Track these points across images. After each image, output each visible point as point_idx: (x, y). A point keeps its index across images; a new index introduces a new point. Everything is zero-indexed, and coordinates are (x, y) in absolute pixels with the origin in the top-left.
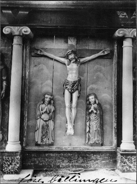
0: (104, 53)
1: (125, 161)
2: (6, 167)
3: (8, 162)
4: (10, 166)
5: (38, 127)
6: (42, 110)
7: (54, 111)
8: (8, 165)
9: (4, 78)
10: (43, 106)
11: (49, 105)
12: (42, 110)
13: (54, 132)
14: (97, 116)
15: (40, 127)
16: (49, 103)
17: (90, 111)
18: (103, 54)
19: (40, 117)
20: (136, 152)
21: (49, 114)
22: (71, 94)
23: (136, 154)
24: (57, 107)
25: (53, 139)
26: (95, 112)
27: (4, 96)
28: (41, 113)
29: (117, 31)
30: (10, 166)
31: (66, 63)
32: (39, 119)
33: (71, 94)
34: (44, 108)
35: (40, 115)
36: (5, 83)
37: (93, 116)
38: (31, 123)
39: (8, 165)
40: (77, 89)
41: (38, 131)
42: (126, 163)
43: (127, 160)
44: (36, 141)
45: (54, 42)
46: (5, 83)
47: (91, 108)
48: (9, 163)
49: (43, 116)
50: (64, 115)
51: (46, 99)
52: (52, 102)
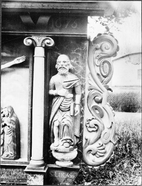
43: (33, 177)
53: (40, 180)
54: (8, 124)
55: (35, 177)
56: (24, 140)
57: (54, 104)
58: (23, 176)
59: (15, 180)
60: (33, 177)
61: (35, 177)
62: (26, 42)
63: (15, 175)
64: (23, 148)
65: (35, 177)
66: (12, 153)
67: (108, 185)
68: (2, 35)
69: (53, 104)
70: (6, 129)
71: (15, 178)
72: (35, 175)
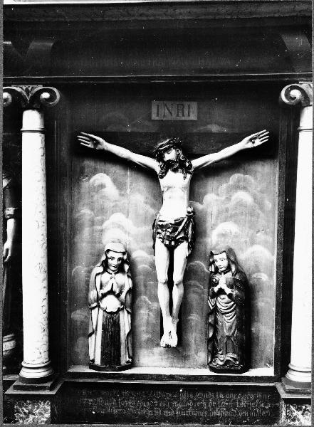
0: (254, 143)
1: (295, 414)
2: (21, 418)
3: (24, 408)
4: (31, 416)
5: (94, 328)
6: (101, 288)
7: (133, 292)
8: (25, 413)
9: (10, 211)
10: (106, 277)
11: (120, 275)
12: (101, 288)
13: (133, 338)
14: (233, 303)
15: (98, 328)
16: (120, 269)
17: (216, 289)
18: (250, 145)
19: (99, 306)
20: (310, 397)
21: (118, 296)
22: (171, 250)
23: (309, 400)
24: (140, 278)
25: (129, 355)
26: (228, 291)
27: (9, 255)
28: (100, 295)
29: (287, 86)
30: (31, 416)
31: (158, 170)
32: (97, 309)
33: (171, 250)
34: (107, 283)
35: (99, 299)
36: (11, 224)
37: (224, 301)
38: (78, 315)
39: (25, 413)
40: (185, 238)
41: (93, 336)
42: (299, 420)
43: (301, 412)
44: (91, 358)
45: (80, 216)
46: (11, 224)
47: (218, 283)
48: (27, 411)
49: (104, 303)
50: (155, 298)
51: (110, 261)
52: (126, 267)
53: (43, 412)
54: (228, 291)
55: (304, 412)
56: (266, 330)
57: (4, 273)
58: (264, 409)
59: (246, 419)
60: (301, 412)
61: (304, 412)
62: (287, 95)
63: (246, 409)
64: (258, 344)
65: (305, 410)
66: (235, 356)
67: (297, 423)
68: (4, 136)
69: (6, 272)
70: (223, 302)
71: (246, 414)
72: (304, 407)
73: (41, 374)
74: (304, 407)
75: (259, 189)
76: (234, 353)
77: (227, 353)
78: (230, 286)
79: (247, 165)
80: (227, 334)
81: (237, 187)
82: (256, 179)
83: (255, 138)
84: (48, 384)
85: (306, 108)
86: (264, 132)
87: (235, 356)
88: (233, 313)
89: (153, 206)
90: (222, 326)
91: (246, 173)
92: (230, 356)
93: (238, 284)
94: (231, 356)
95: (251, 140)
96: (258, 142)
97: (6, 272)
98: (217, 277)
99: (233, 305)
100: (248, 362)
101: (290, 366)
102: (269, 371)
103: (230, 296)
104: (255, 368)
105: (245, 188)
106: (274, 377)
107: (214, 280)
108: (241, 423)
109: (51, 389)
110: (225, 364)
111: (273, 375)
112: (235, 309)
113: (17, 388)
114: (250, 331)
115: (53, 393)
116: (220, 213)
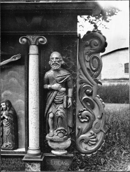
14: (8, 122)
18: (14, 60)
26: (6, 117)
42: (30, 169)
54: (6, 117)
55: (32, 166)
61: (32, 166)
62: (21, 41)
65: (33, 165)
66: (10, 143)
69: (47, 97)
72: (32, 164)
73: (35, 152)
74: (32, 164)
75: (20, 77)
76: (10, 142)
77: (7, 142)
78: (8, 116)
79: (15, 67)
80: (6, 135)
81: (11, 76)
82: (18, 73)
83: (16, 57)
84: (40, 156)
85: (30, 46)
86: (19, 55)
87: (10, 143)
88: (9, 126)
89: (87, 68)
90: (5, 131)
91: (15, 70)
92: (8, 143)
93: (10, 115)
94: (8, 143)
95: (14, 57)
96: (17, 59)
97: (47, 97)
98: (2, 112)
99: (9, 123)
100: (16, 146)
101: (29, 148)
102: (23, 150)
103: (7, 119)
104: (21, 148)
105: (14, 77)
106: (25, 152)
107: (1, 113)
108: (12, 170)
109: (41, 158)
110: (6, 147)
111: (25, 151)
112: (9, 125)
113: (26, 158)
114: (18, 134)
115: (42, 160)
116: (4, 86)
